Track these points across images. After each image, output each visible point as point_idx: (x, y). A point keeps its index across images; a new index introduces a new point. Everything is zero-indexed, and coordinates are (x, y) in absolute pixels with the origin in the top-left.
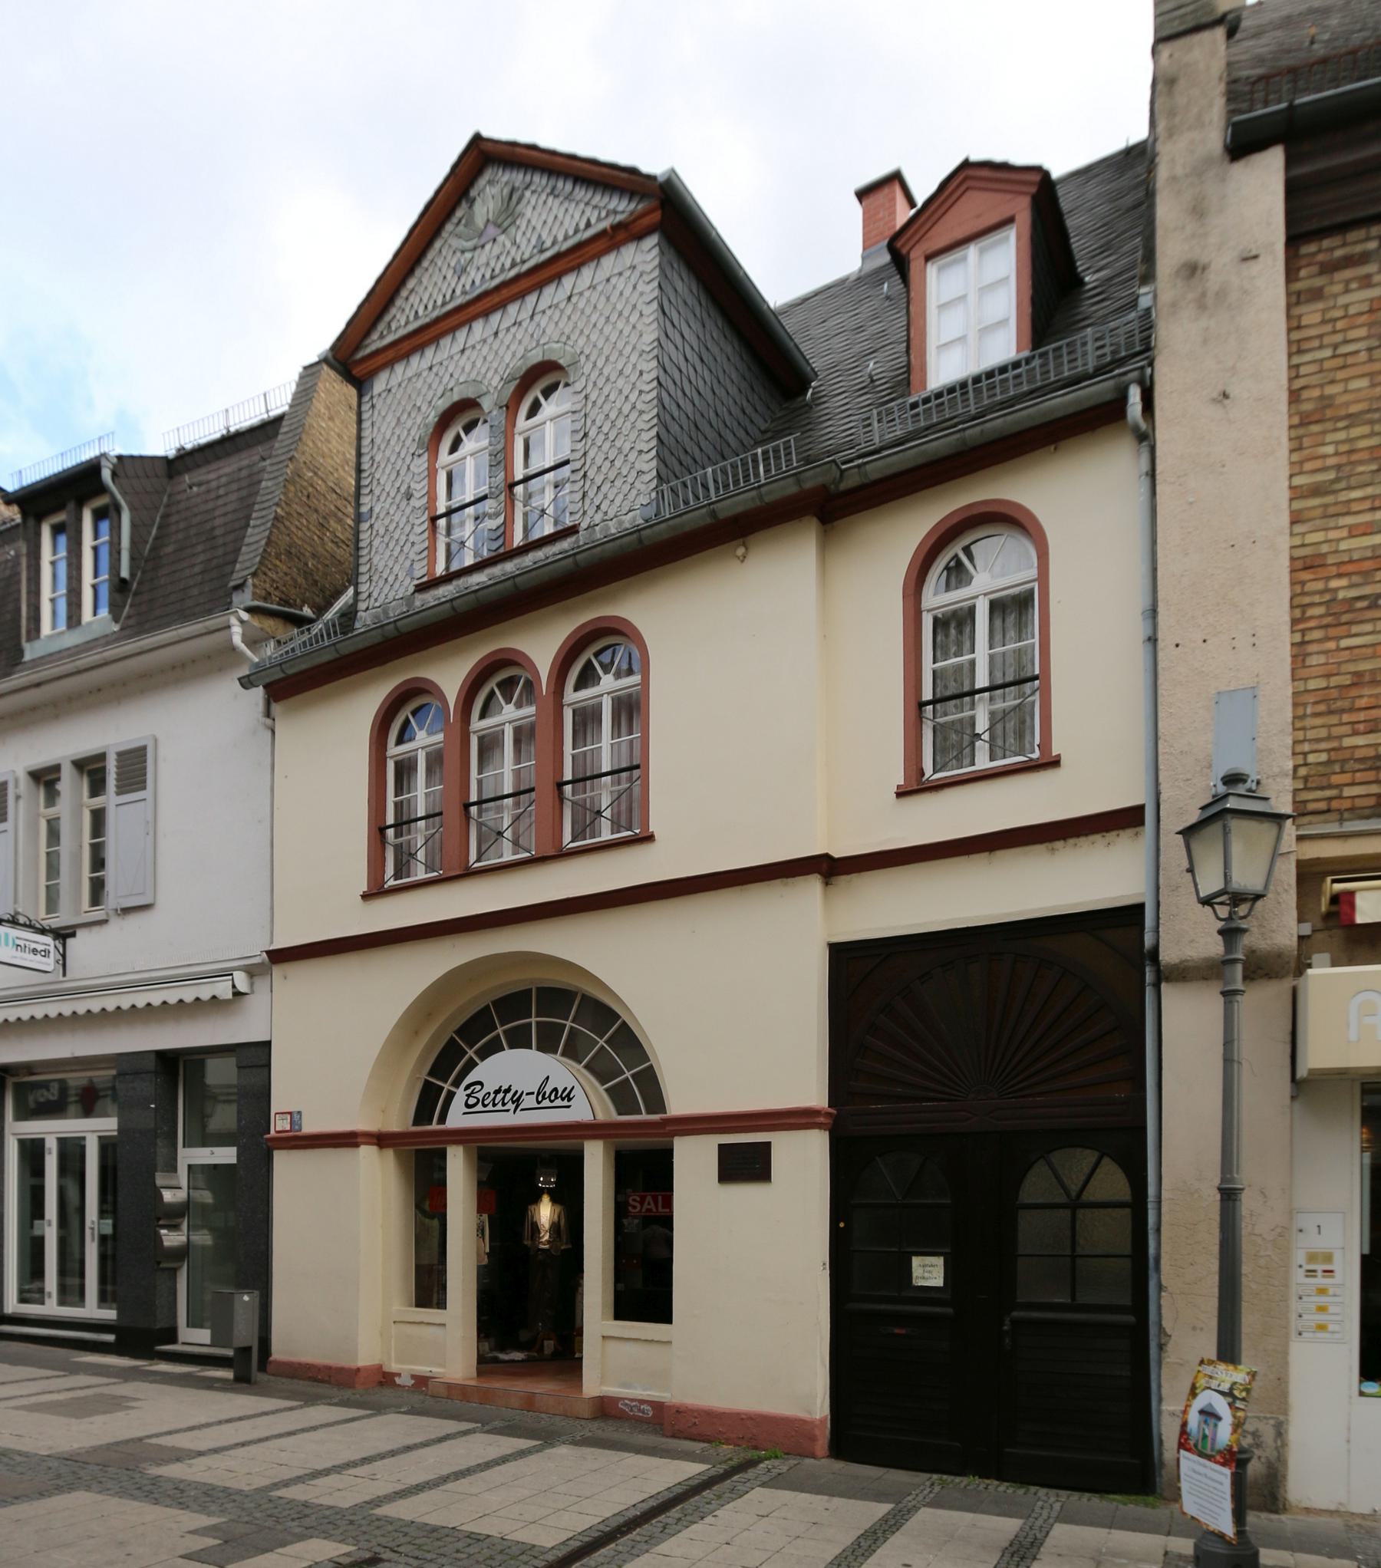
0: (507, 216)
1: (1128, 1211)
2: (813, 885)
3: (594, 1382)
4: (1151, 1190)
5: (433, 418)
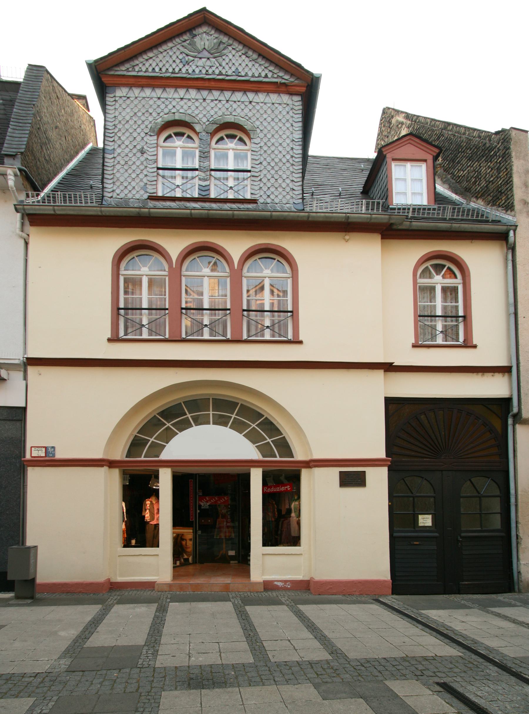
0: (216, 52)
1: (462, 495)
2: (380, 374)
3: (257, 575)
4: (512, 491)
5: (160, 121)
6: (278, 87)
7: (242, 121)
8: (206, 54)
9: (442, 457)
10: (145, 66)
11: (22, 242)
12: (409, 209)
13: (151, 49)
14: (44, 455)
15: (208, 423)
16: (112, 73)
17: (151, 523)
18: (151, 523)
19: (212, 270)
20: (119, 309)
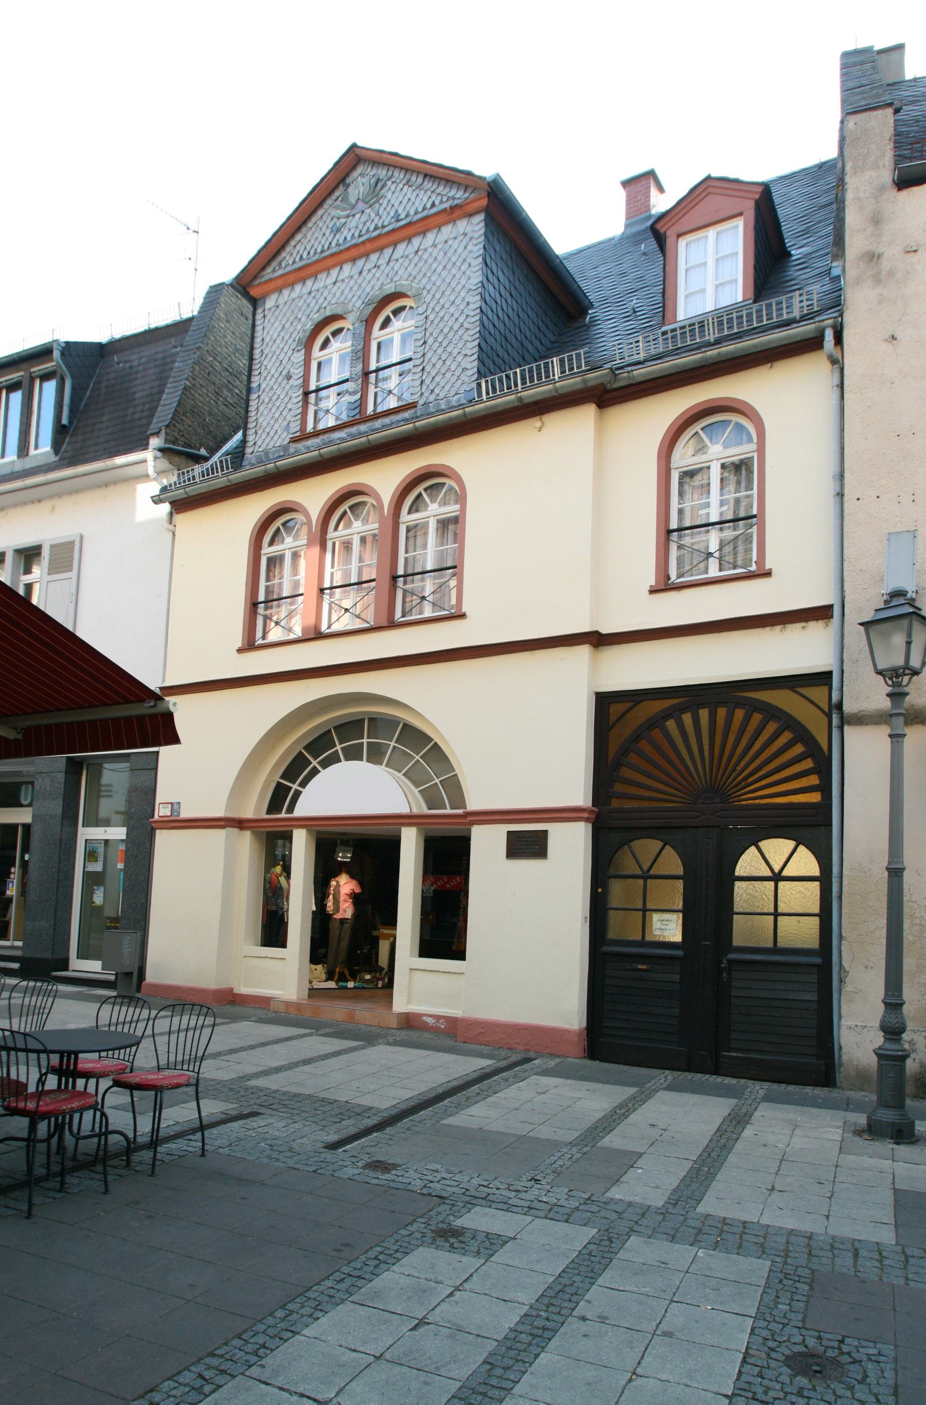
2: (584, 651)
6: (452, 213)
7: (390, 289)
8: (361, 205)
9: (700, 801)
10: (291, 258)
11: (171, 534)
12: (702, 325)
13: (299, 229)
14: (169, 814)
15: (339, 761)
16: (257, 282)
17: (335, 916)
18: (335, 916)
19: (363, 524)
20: (669, 532)
